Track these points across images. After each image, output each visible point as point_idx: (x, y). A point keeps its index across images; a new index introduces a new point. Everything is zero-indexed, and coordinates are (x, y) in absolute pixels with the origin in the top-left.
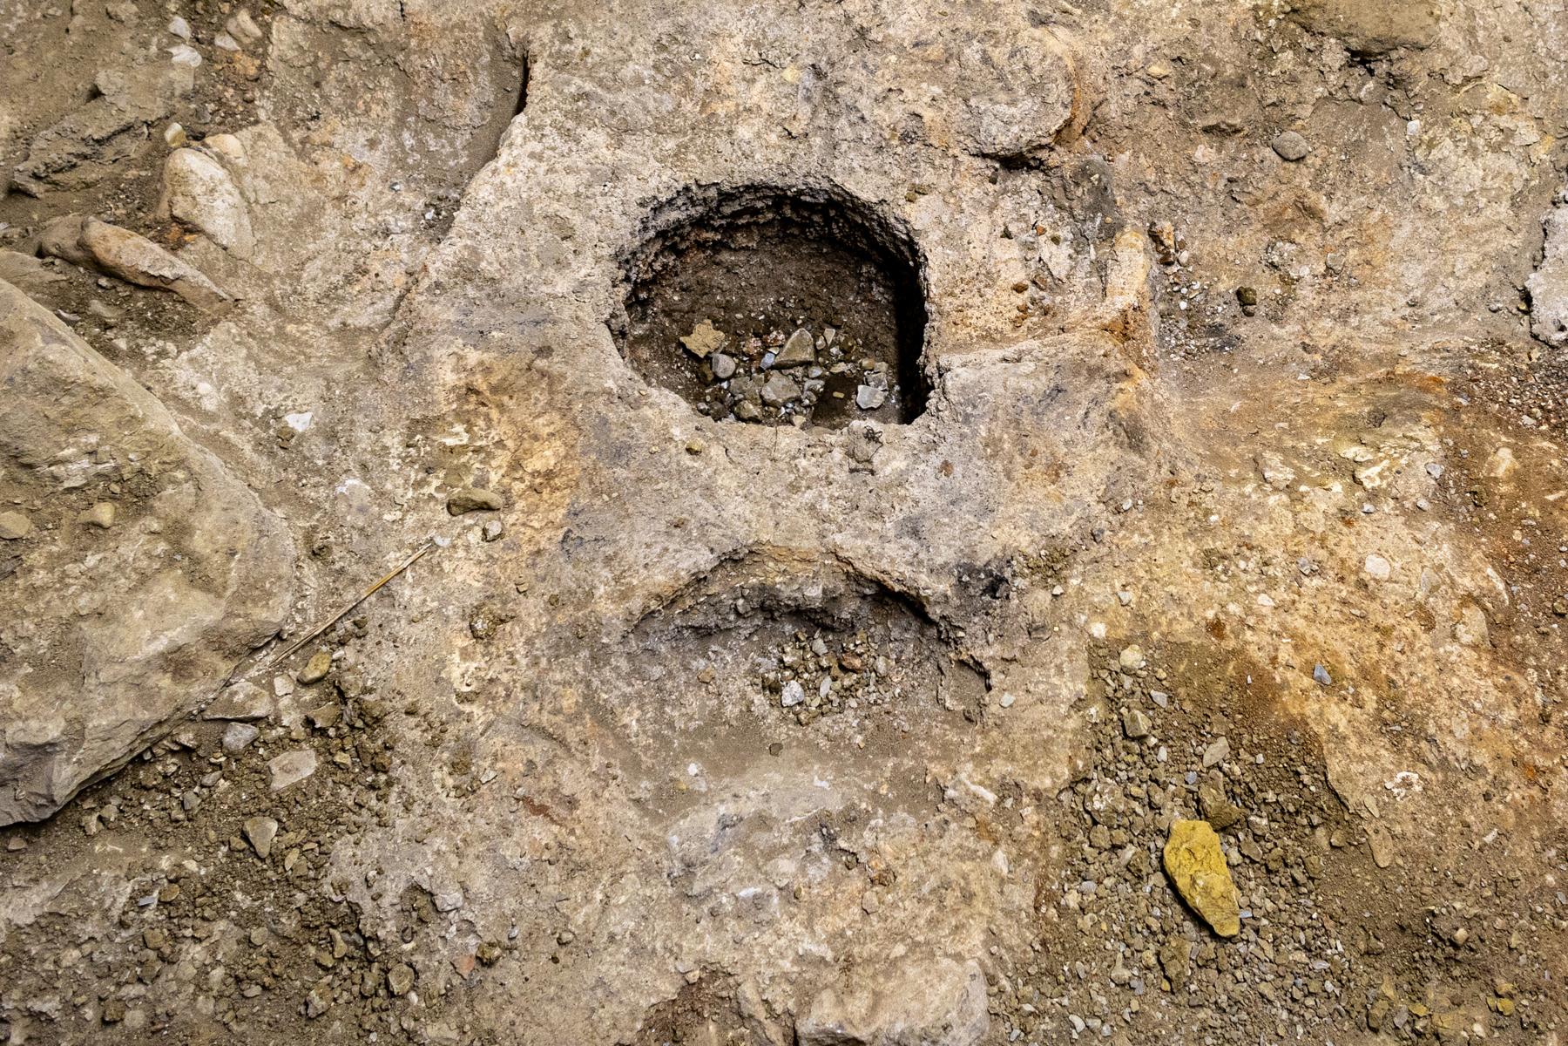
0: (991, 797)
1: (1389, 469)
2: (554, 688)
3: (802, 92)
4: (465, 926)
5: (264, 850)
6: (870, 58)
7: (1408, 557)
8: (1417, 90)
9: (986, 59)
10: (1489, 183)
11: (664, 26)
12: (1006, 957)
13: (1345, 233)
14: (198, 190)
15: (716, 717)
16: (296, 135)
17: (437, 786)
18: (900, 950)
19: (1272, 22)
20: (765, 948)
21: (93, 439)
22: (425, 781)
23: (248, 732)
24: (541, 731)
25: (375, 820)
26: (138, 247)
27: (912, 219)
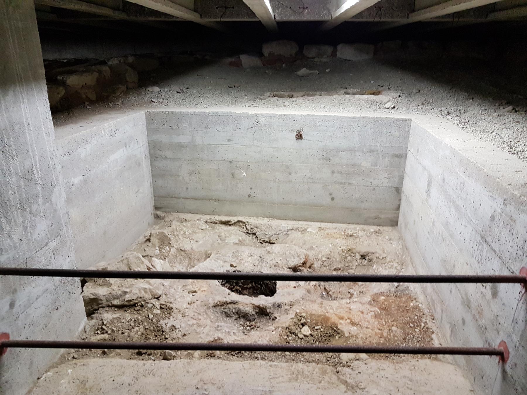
9: (290, 253)
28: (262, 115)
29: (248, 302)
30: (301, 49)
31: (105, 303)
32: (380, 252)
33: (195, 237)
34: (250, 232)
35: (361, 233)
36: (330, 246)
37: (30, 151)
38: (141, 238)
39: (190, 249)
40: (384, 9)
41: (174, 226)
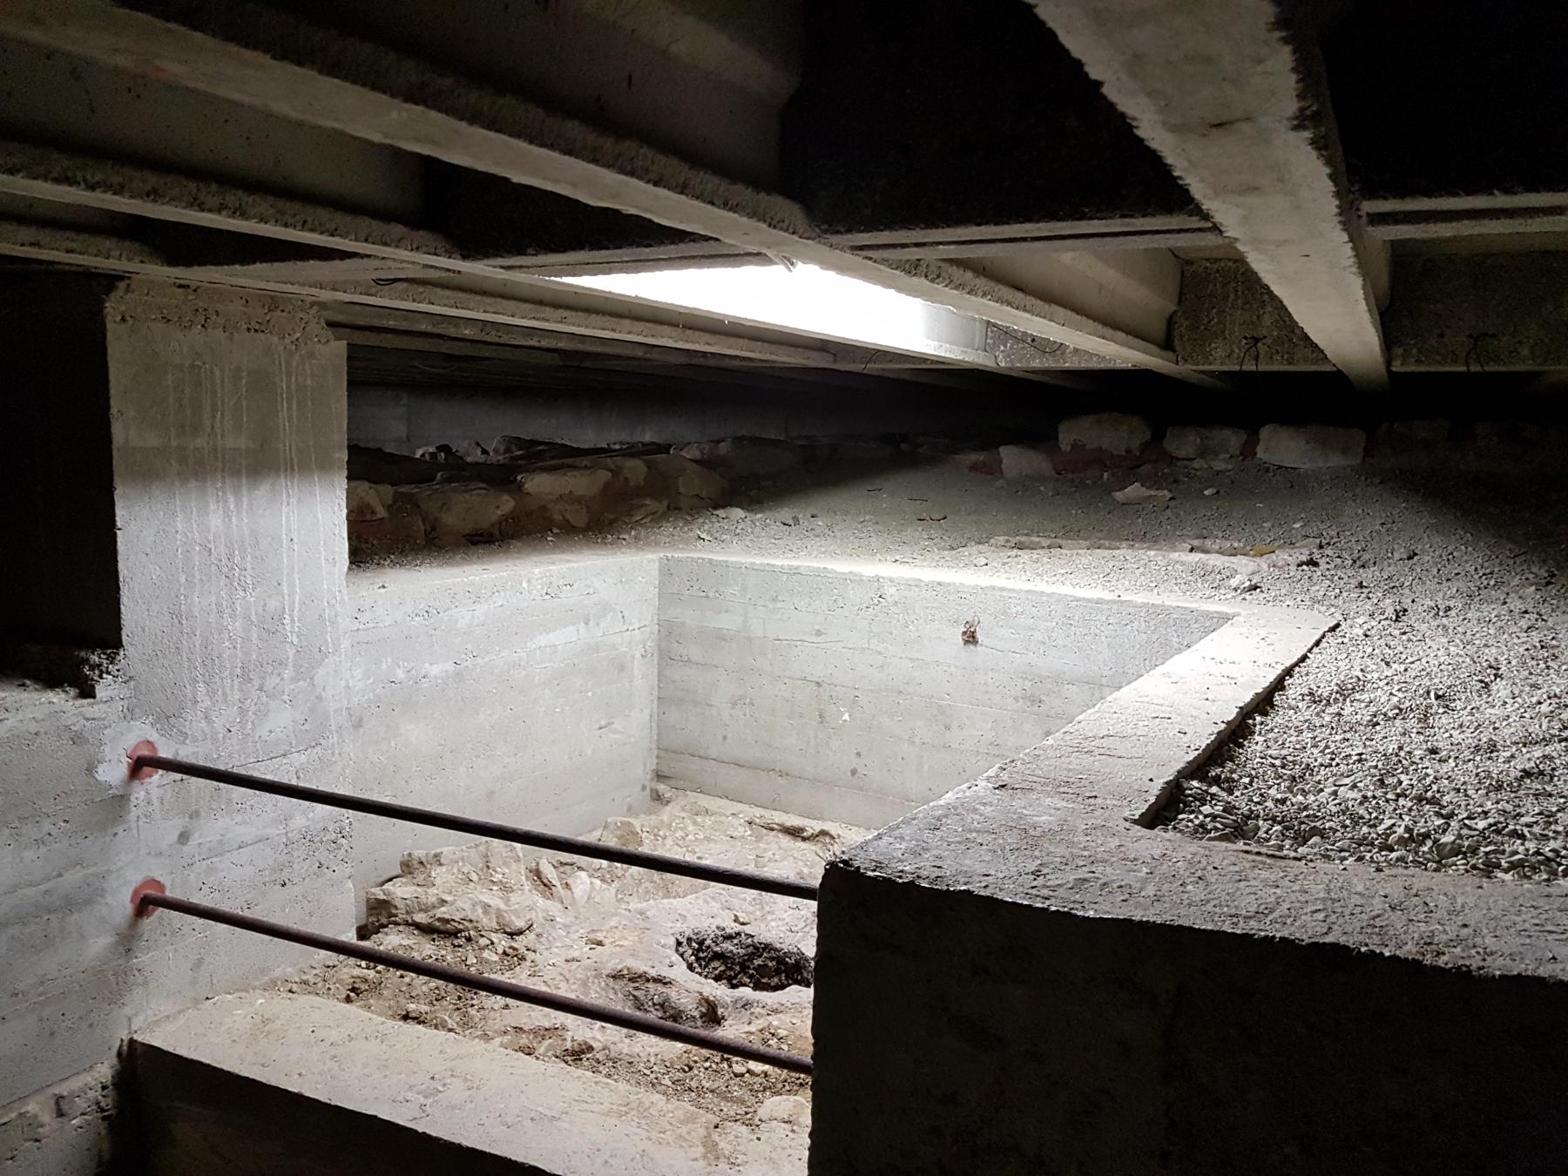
28: (891, 580)
29: (689, 985)
30: (1158, 437)
31: (401, 917)
37: (285, 584)
40: (1269, 341)
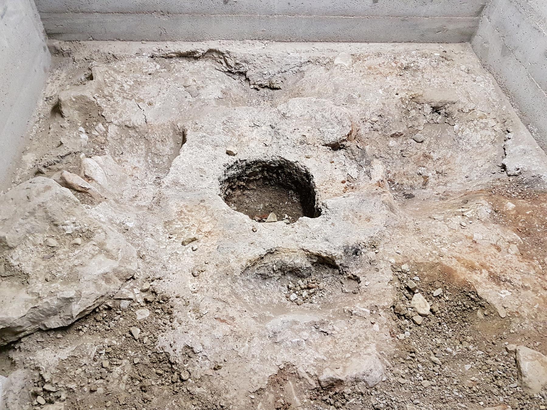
0: (368, 311)
1: (474, 211)
2: (222, 288)
3: (268, 133)
4: (204, 357)
5: (137, 337)
6: (287, 121)
7: (486, 234)
8: (455, 116)
10: (483, 139)
11: (224, 119)
12: (385, 353)
13: (441, 162)
14: (92, 169)
15: (271, 302)
16: (117, 159)
17: (189, 317)
18: (348, 355)
19: (407, 102)
20: (304, 357)
21: (74, 219)
22: (185, 316)
23: (128, 302)
24: (219, 300)
25: (171, 328)
26: (78, 178)
27: (307, 165)
32: (464, 100)
33: (142, 93)
34: (234, 71)
35: (422, 63)
36: (381, 91)
38: (41, 103)
39: (144, 122)
41: (98, 78)
